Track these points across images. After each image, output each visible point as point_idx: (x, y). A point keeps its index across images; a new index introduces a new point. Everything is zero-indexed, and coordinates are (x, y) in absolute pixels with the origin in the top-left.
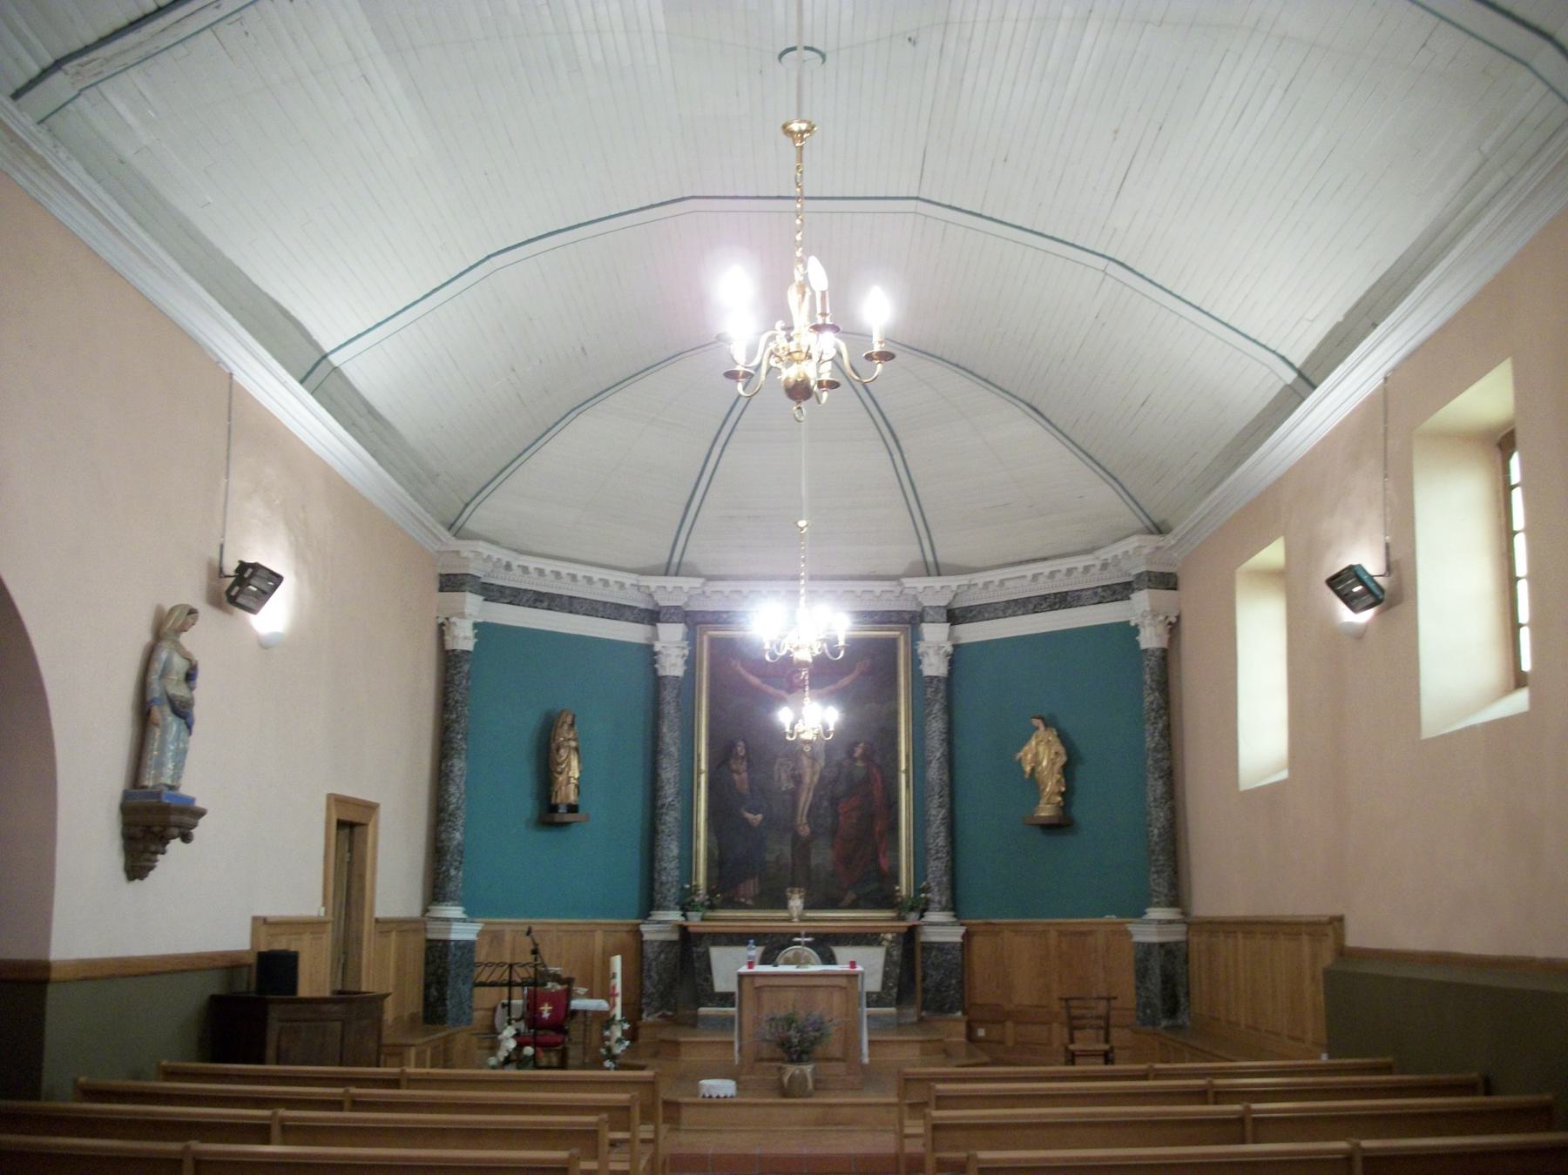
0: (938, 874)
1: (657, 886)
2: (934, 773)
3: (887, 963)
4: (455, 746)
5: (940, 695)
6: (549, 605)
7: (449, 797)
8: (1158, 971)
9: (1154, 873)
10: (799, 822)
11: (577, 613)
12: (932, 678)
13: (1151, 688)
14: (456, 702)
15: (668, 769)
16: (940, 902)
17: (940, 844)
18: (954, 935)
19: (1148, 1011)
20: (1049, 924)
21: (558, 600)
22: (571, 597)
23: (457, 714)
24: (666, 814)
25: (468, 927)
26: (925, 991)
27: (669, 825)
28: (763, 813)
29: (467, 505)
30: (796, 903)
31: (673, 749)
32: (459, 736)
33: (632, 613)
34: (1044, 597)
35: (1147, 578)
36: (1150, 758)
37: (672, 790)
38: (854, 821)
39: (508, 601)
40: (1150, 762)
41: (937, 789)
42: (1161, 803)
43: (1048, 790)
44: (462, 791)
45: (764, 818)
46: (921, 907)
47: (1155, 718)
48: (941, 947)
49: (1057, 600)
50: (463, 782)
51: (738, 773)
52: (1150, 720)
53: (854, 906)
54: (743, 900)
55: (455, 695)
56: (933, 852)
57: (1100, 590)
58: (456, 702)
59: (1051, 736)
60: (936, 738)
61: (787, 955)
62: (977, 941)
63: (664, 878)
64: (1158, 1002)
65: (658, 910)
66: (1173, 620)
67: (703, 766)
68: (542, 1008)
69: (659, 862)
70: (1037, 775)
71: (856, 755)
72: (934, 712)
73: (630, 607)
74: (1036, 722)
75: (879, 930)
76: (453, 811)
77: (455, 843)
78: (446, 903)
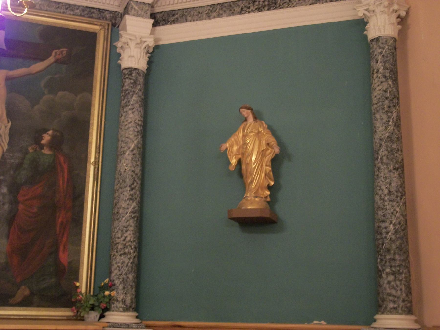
0: (125, 270)
5: (139, 87)
12: (131, 70)
13: (385, 77)
16: (124, 302)
17: (128, 239)
36: (383, 148)
38: (35, 210)
41: (128, 182)
42: (397, 197)
46: (103, 305)
47: (389, 107)
49: (266, 3)
52: (383, 109)
56: (120, 246)
60: (132, 129)
65: (383, 313)
66: (403, 14)
70: (244, 167)
71: (43, 142)
72: (132, 102)
74: (246, 112)
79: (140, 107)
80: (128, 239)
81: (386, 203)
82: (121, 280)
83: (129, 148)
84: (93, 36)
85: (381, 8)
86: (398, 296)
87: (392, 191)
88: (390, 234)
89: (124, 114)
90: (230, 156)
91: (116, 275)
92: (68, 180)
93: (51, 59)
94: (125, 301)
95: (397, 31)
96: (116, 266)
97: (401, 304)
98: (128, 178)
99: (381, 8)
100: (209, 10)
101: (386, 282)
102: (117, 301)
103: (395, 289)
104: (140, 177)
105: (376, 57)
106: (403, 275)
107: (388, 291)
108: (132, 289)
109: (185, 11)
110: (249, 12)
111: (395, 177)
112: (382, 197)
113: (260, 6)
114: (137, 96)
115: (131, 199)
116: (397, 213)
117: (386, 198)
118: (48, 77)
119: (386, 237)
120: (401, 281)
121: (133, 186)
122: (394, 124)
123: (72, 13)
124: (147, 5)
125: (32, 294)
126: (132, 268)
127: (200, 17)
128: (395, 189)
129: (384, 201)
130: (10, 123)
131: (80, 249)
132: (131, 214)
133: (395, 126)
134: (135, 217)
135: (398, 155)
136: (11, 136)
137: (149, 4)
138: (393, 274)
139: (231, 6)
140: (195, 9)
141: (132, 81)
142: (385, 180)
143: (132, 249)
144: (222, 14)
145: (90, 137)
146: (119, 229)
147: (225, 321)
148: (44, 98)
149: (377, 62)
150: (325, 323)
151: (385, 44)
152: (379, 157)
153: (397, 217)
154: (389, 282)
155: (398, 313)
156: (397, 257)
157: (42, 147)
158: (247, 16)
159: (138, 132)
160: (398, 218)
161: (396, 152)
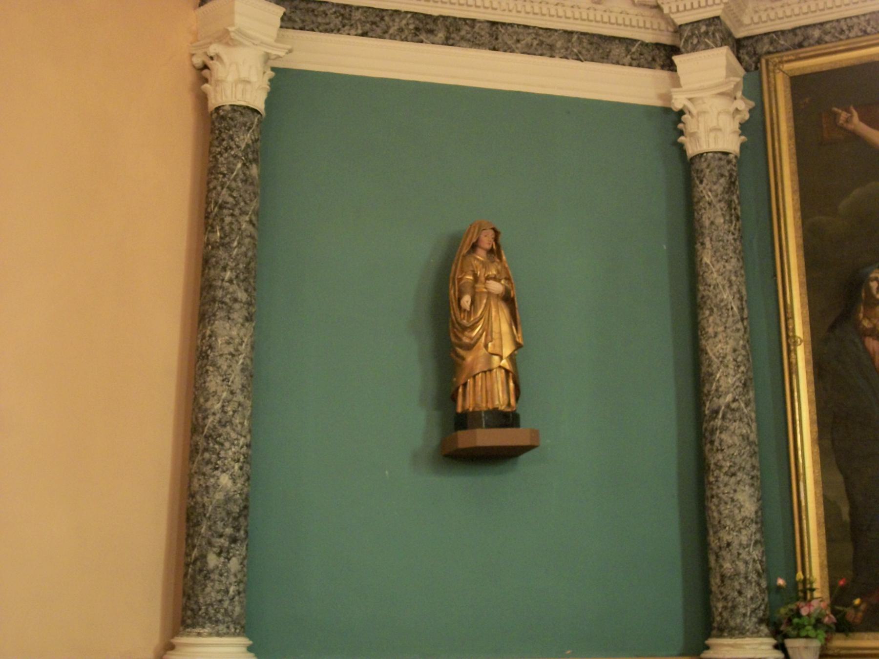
1: (715, 581)
4: (220, 293)
6: (447, 38)
7: (207, 400)
11: (510, 50)
15: (720, 337)
22: (493, 24)
23: (222, 229)
24: (723, 429)
32: (228, 275)
33: (628, 51)
37: (730, 380)
44: (237, 385)
50: (238, 367)
55: (219, 194)
58: (221, 207)
63: (727, 565)
65: (721, 636)
67: (800, 328)
69: (715, 533)
73: (621, 40)
76: (214, 428)
77: (219, 496)
78: (198, 630)
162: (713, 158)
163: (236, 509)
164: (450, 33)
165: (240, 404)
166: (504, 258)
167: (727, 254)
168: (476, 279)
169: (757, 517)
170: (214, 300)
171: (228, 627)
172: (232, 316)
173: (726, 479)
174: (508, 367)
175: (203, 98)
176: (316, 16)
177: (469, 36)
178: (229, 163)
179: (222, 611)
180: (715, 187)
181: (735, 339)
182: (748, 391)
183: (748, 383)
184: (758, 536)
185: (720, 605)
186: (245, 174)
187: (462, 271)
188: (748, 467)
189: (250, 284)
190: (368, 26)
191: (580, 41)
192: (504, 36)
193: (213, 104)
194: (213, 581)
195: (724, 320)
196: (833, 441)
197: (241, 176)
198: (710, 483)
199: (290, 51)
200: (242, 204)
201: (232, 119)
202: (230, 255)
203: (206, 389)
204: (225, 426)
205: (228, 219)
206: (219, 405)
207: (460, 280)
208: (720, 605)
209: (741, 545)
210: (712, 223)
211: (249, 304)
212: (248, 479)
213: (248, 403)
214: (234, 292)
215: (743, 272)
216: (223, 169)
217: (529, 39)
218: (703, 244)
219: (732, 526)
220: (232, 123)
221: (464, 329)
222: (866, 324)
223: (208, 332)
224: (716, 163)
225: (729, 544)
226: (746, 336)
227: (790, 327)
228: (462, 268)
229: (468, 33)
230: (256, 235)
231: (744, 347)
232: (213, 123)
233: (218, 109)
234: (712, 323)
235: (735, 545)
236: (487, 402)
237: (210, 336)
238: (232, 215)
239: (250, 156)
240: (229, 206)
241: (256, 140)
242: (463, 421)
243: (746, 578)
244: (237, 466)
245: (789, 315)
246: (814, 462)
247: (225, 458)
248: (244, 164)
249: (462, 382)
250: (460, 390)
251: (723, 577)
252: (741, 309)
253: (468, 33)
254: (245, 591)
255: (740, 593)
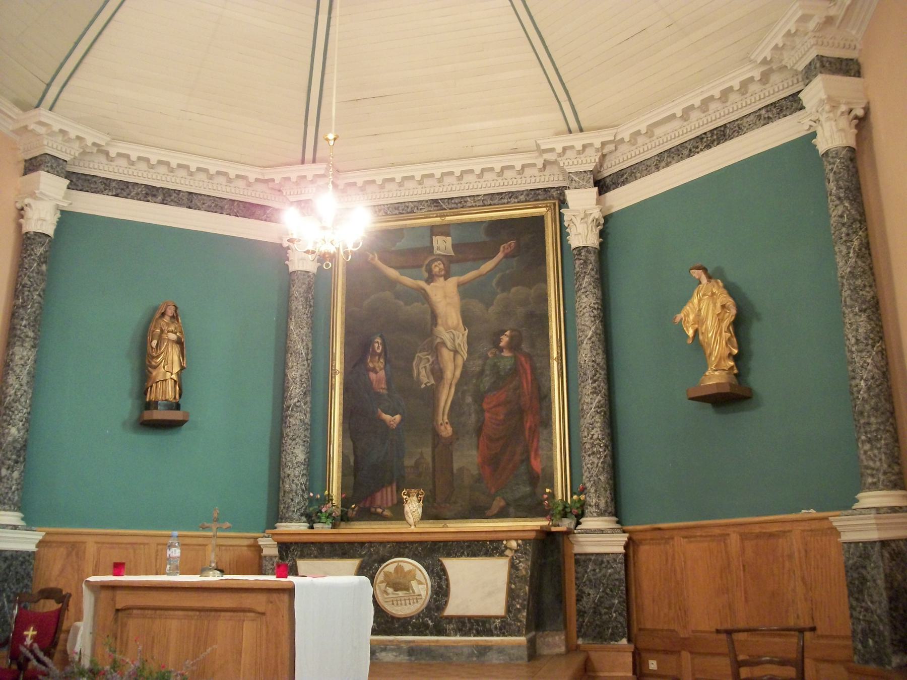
0: (595, 471)
2: (587, 354)
3: (512, 578)
4: (18, 332)
7: (7, 388)
8: (881, 583)
9: (863, 442)
10: (440, 422)
13: (839, 198)
14: (24, 286)
16: (597, 506)
17: (595, 437)
18: (615, 544)
19: (871, 642)
20: (727, 525)
21: (175, 195)
22: (190, 193)
23: (23, 298)
24: (291, 416)
25: (16, 536)
26: (581, 613)
27: (292, 428)
28: (400, 414)
29: (49, 85)
30: (413, 507)
31: (300, 347)
32: (24, 323)
34: (700, 138)
35: (818, 65)
36: (846, 287)
39: (114, 193)
40: (846, 293)
41: (590, 374)
42: (867, 345)
43: (715, 353)
45: (402, 420)
47: (848, 235)
48: (599, 559)
49: (715, 137)
50: (26, 372)
51: (374, 370)
52: (841, 238)
53: (502, 514)
54: (379, 510)
55: (22, 279)
56: (588, 446)
57: (763, 112)
58: (24, 286)
59: (717, 287)
60: (587, 314)
61: (386, 569)
62: (647, 554)
63: (287, 486)
64: (885, 629)
65: (281, 522)
68: (25, 633)
69: (283, 469)
70: (701, 337)
71: (502, 344)
72: (584, 286)
74: (696, 273)
75: (500, 536)
76: (10, 403)
77: (10, 439)
79: (594, 288)
80: (595, 437)
81: (854, 356)
82: (592, 482)
83: (586, 337)
84: (540, 219)
85: (825, 115)
86: (876, 468)
87: (859, 338)
88: (861, 393)
89: (578, 300)
90: (686, 327)
91: (587, 477)
92: (532, 380)
93: (500, 255)
94: (598, 506)
95: (316, 267)
96: (585, 468)
97: (882, 477)
98: (589, 369)
99: (825, 115)
100: (657, 160)
101: (862, 452)
102: (590, 506)
103: (872, 460)
104: (605, 366)
105: (828, 176)
106: (883, 442)
107: (865, 463)
108: (606, 491)
109: (632, 168)
110: (698, 153)
111: (862, 321)
112: (850, 349)
113: (709, 142)
114: (589, 276)
115: (595, 392)
116: (868, 364)
117: (853, 349)
118: (498, 276)
119: (858, 398)
120: (879, 449)
121: (595, 378)
122: (856, 254)
123: (516, 201)
124: (589, 173)
125: (508, 504)
126: (603, 468)
127: (649, 171)
128: (863, 335)
129: (852, 352)
130: (467, 331)
131: (552, 454)
132: (595, 410)
133: (857, 256)
134: (601, 411)
135: (864, 293)
136: (469, 343)
137: (591, 171)
138: (869, 442)
139: (678, 150)
140: (643, 163)
141: (582, 261)
142: (851, 327)
143: (601, 447)
144: (670, 162)
145: (550, 331)
146: (585, 427)
147: (707, 519)
148: (498, 296)
149: (829, 182)
150: (814, 512)
151: (835, 157)
152: (843, 299)
153: (869, 370)
154: (865, 452)
155: (878, 489)
156: (873, 420)
157: (501, 350)
158: (697, 156)
159: (594, 317)
160: (870, 371)
161: (861, 290)
162: (300, 274)
163: (19, 446)
164: (165, 197)
165: (25, 391)
166: (180, 321)
167: (302, 325)
168: (162, 331)
169: (305, 462)
170: (15, 336)
171: (10, 507)
172: (24, 345)
173: (291, 441)
174: (175, 379)
175: (20, 226)
176: (90, 183)
177: (176, 199)
178: (30, 263)
179: (7, 498)
180: (300, 290)
181: (302, 370)
182: (306, 397)
183: (307, 393)
184: (305, 472)
185: (282, 506)
186: (38, 269)
187: (155, 327)
188: (302, 436)
189: (36, 328)
190: (119, 191)
191: (239, 206)
192: (196, 201)
193: (24, 230)
194: (4, 483)
195: (297, 359)
196: (349, 424)
197: (36, 270)
198: (283, 444)
199: (71, 204)
200: (35, 285)
201: (33, 239)
202: (26, 312)
203: (7, 383)
204: (16, 402)
205: (27, 293)
206: (13, 391)
207: (153, 331)
208: (282, 506)
209: (295, 475)
210: (296, 308)
211: (35, 339)
212: (27, 431)
213: (30, 391)
214: (27, 332)
215: (310, 335)
216: (26, 266)
217: (209, 203)
218: (291, 319)
219: (291, 466)
220: (34, 242)
221: (153, 357)
222: (371, 365)
223: (11, 353)
224: (302, 277)
225: (289, 475)
226: (309, 369)
227: (334, 364)
228: (155, 326)
229: (175, 198)
230: (42, 301)
231: (307, 374)
232: (24, 240)
233: (27, 233)
234: (292, 361)
235: (292, 475)
236: (162, 396)
237: (12, 355)
238: (29, 291)
239: (42, 260)
240: (28, 286)
241: (47, 251)
242: (150, 406)
243: (296, 493)
244: (21, 424)
245: (334, 359)
246: (339, 435)
247: (15, 419)
248: (38, 264)
249: (149, 385)
250: (149, 389)
251: (285, 492)
252: (307, 354)
253: (175, 198)
254: (21, 489)
255: (292, 500)
